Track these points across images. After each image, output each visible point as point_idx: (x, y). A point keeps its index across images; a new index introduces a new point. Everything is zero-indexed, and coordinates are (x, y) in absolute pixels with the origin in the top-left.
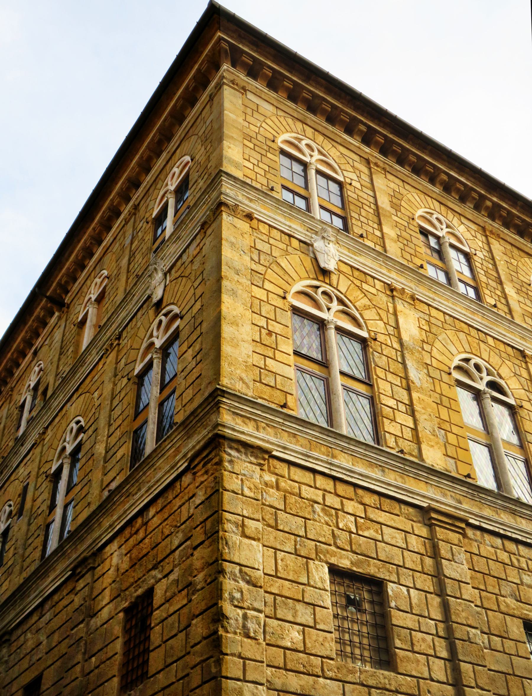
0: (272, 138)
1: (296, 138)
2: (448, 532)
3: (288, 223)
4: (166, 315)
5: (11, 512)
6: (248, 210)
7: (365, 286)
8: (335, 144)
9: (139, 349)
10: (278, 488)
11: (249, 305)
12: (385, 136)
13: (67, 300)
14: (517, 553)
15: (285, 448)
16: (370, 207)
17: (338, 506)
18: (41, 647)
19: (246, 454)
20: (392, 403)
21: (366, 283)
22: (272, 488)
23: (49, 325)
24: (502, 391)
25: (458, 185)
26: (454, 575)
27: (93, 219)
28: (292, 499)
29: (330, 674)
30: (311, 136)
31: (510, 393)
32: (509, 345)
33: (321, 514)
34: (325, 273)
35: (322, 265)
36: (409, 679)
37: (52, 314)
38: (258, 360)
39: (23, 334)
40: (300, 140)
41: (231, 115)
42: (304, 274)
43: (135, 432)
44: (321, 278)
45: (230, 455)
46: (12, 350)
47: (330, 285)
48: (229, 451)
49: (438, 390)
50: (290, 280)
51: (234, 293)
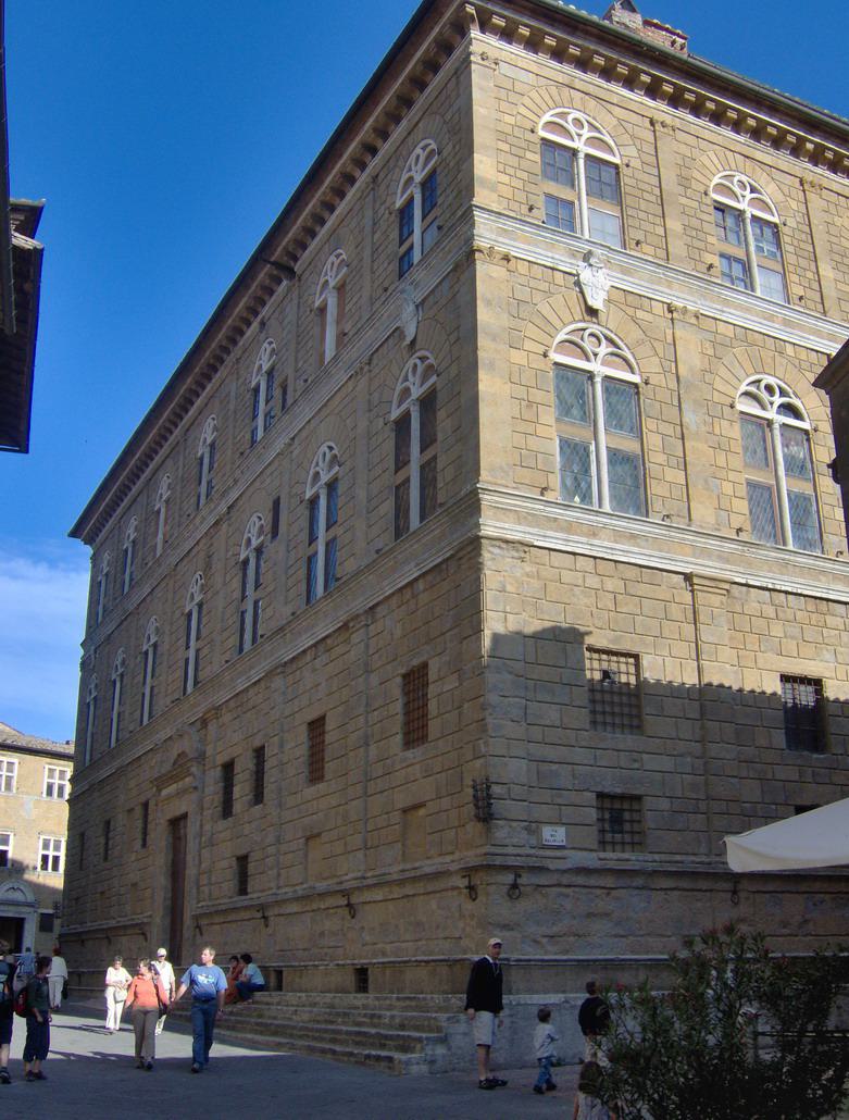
0: (529, 125)
1: (557, 115)
2: (710, 595)
3: (550, 255)
4: (424, 149)
5: (262, 526)
6: (503, 249)
7: (640, 314)
8: (609, 106)
9: (391, 402)
10: (539, 578)
11: (507, 377)
12: (672, 83)
13: (297, 268)
14: (785, 605)
15: (545, 536)
16: (652, 193)
17: (598, 586)
18: (320, 688)
19: (508, 549)
20: (661, 459)
21: (641, 309)
22: (533, 578)
23: (276, 294)
24: (797, 415)
25: (770, 129)
26: (711, 639)
27: (323, 182)
28: (552, 586)
29: (583, 743)
30: (578, 106)
31: (805, 416)
32: (812, 350)
33: (581, 597)
34: (592, 312)
35: (590, 303)
36: (658, 741)
37: (279, 281)
38: (519, 440)
39: (245, 300)
40: (563, 115)
41: (481, 110)
42: (567, 317)
43: (397, 488)
44: (587, 318)
45: (492, 553)
46: (234, 316)
47: (599, 324)
48: (491, 549)
49: (717, 431)
50: (552, 331)
51: (492, 366)
